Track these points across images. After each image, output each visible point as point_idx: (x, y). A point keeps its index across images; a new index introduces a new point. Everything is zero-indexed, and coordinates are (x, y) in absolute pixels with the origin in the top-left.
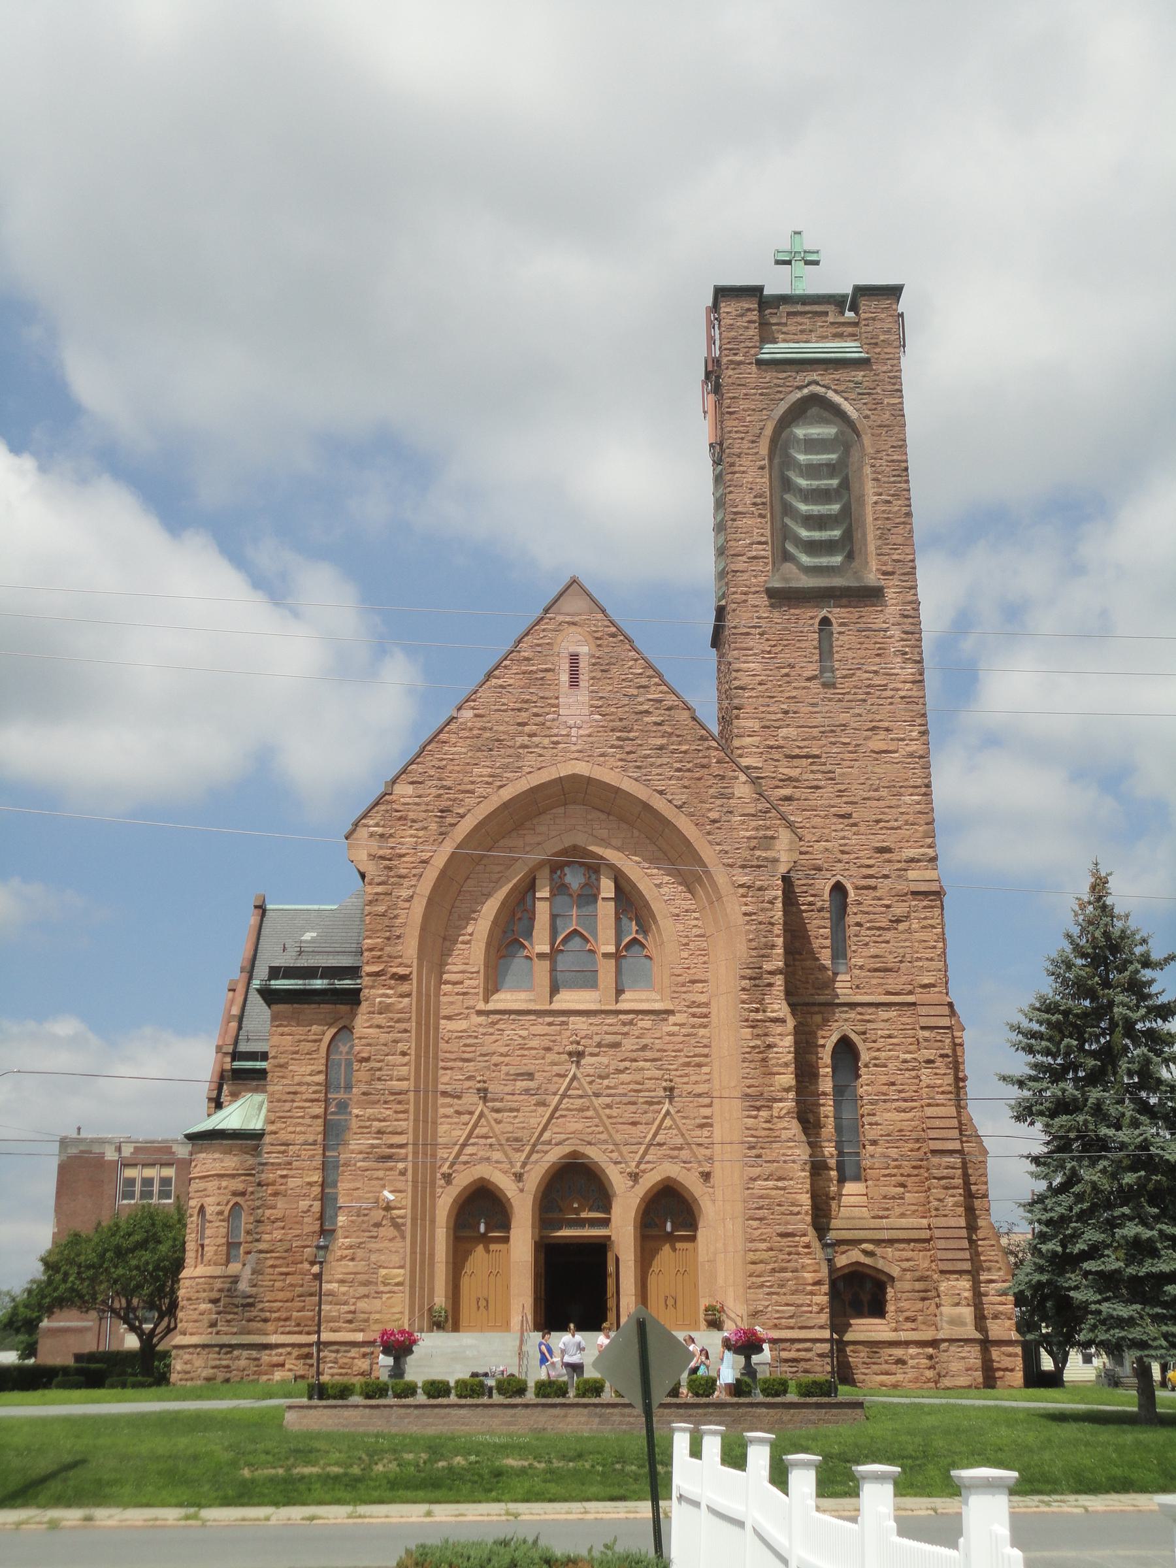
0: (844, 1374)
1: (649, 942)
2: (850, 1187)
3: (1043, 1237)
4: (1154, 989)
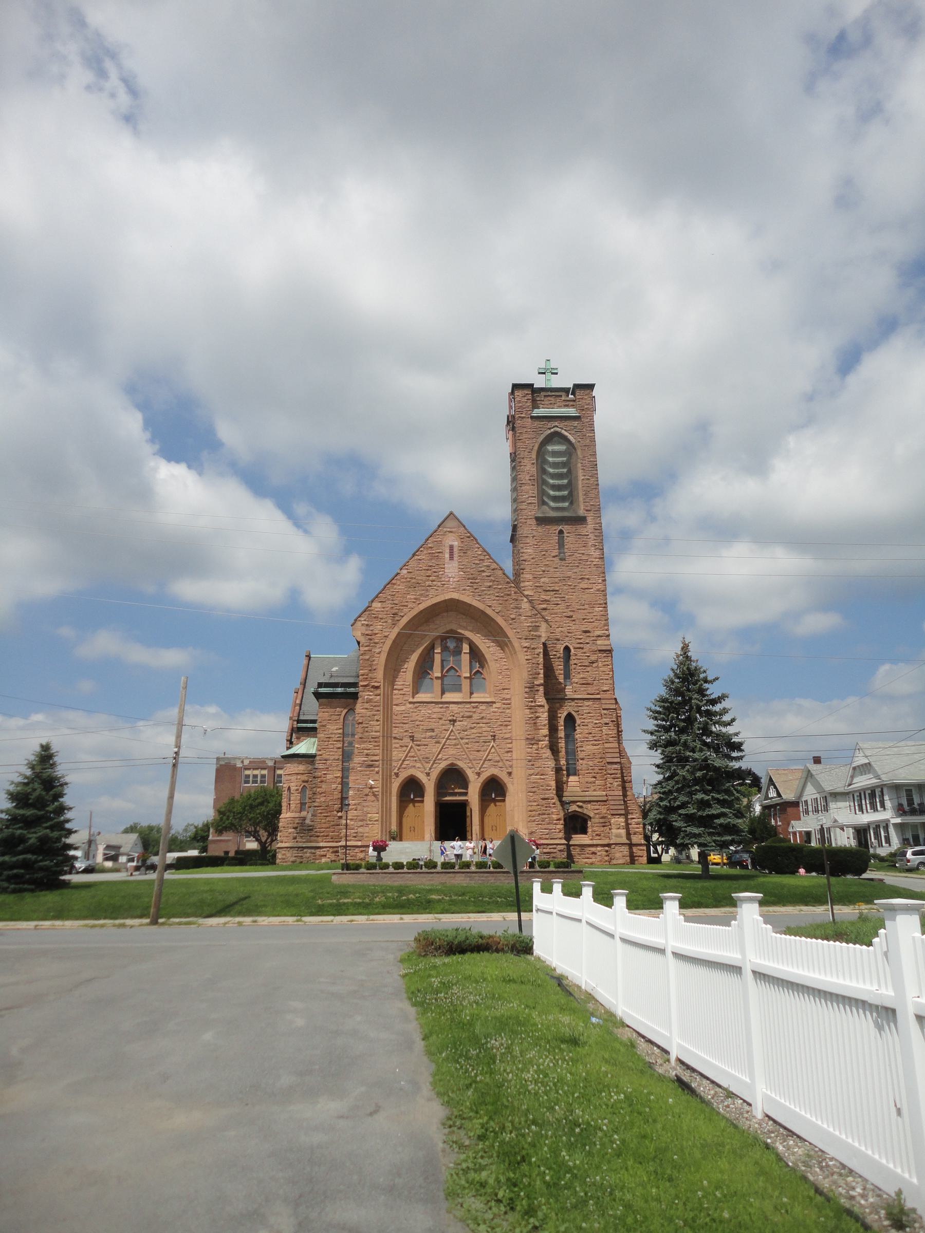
0: (570, 856)
1: (484, 672)
2: (572, 778)
3: (661, 799)
4: (708, 692)
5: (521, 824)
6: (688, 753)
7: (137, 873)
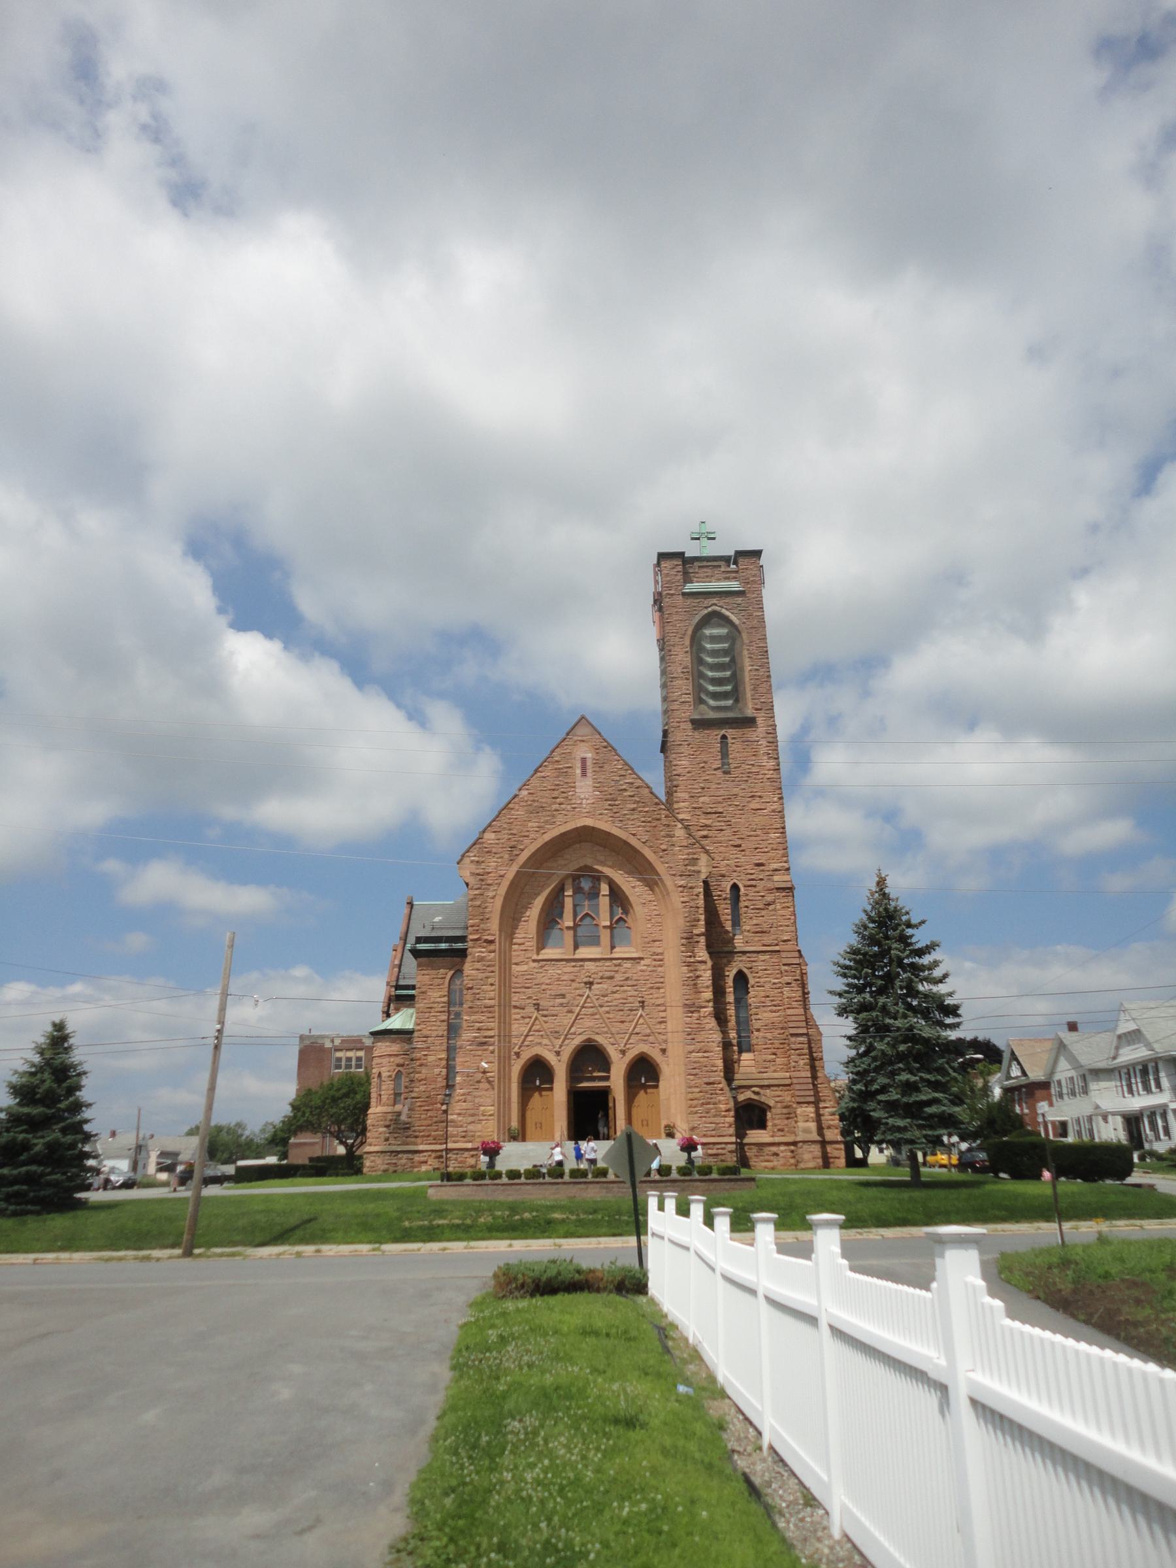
0: (744, 1162)
2: (745, 1056)
3: (854, 1082)
4: (913, 940)
5: (679, 1117)
6: (888, 1021)
7: (183, 1188)
